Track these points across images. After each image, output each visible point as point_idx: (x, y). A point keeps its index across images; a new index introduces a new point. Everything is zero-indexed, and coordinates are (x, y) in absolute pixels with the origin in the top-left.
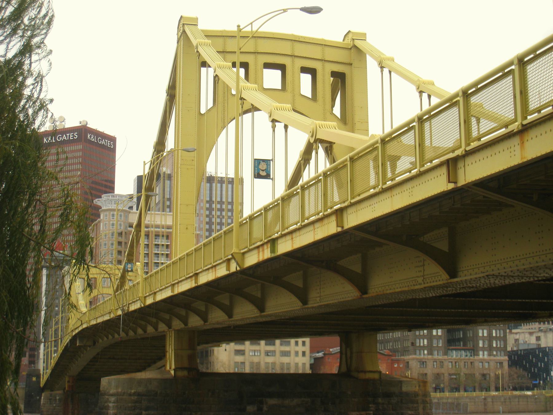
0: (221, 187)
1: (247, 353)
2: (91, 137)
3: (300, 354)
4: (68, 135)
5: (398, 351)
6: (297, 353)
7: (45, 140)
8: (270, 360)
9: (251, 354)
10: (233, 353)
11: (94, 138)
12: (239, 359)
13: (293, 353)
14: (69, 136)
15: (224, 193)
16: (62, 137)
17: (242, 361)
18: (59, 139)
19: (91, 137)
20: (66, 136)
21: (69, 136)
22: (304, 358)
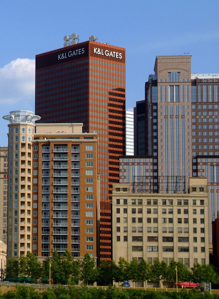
0: (213, 98)
1: (144, 249)
2: (97, 50)
3: (199, 250)
4: (77, 50)
5: (80, 279)
6: (195, 249)
7: (59, 57)
8: (154, 255)
9: (148, 250)
10: (130, 249)
11: (101, 51)
12: (137, 254)
13: (191, 249)
14: (78, 51)
15: (123, 68)
16: (72, 53)
17: (141, 256)
18: (70, 55)
19: (97, 50)
20: (76, 52)
21: (78, 51)
22: (203, 254)
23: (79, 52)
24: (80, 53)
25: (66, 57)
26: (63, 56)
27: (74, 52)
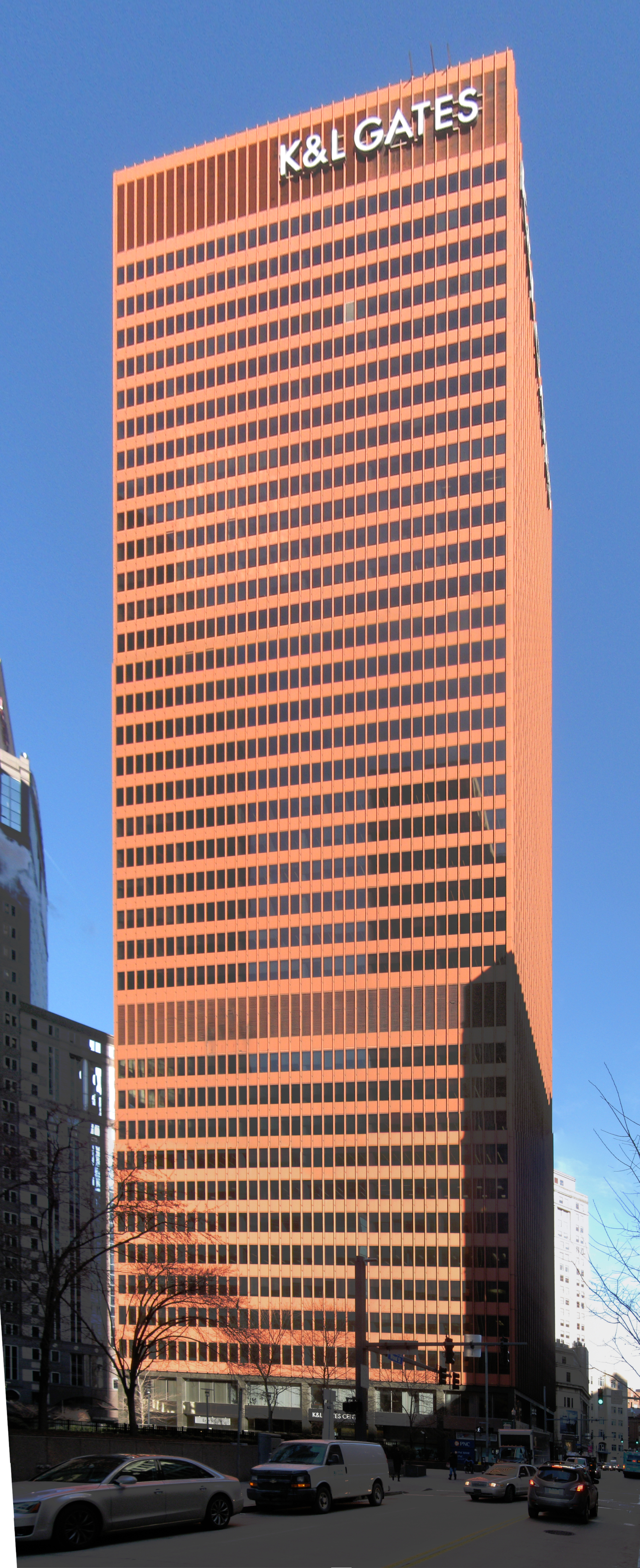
23: (439, 113)
24: (444, 118)
25: (336, 156)
26: (312, 149)
27: (399, 116)
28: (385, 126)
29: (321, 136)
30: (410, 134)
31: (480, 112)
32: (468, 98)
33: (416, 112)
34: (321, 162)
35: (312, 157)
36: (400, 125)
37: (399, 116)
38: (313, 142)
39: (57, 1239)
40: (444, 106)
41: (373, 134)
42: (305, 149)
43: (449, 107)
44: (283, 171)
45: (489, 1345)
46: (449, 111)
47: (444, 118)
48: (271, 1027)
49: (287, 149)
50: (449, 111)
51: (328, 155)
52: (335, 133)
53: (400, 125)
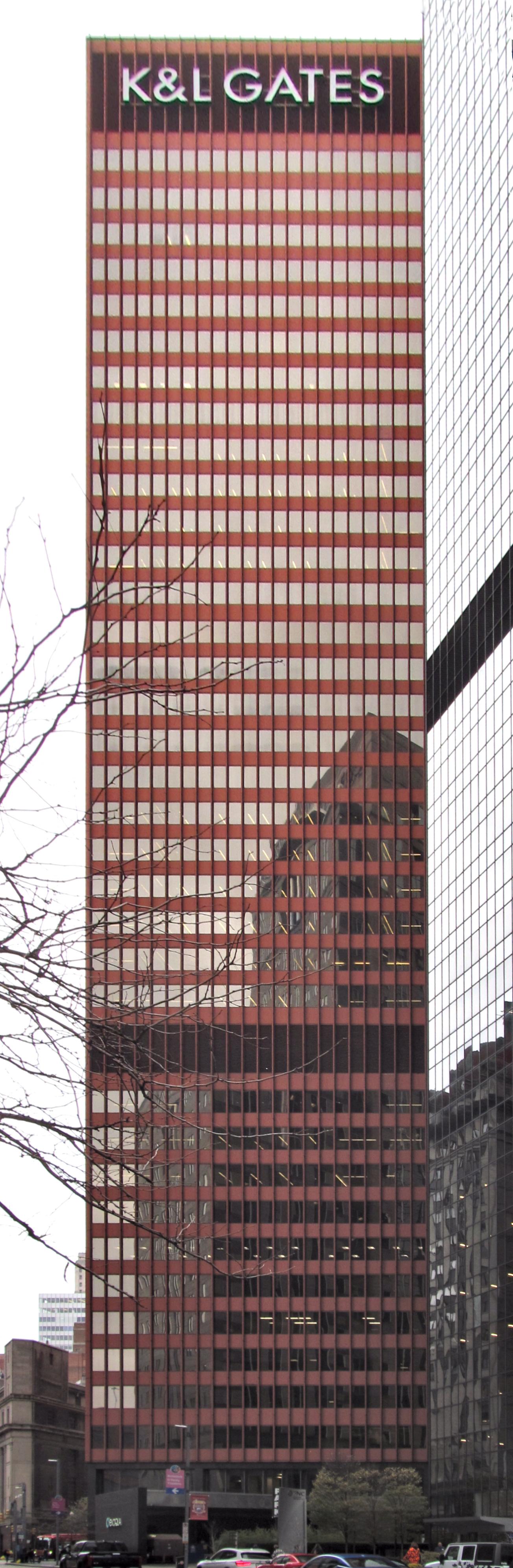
23: (334, 86)
24: (340, 93)
27: (283, 75)
28: (265, 82)
29: (177, 71)
30: (298, 98)
31: (386, 96)
32: (371, 78)
33: (305, 77)
34: (177, 99)
35: (165, 92)
36: (283, 85)
37: (283, 75)
38: (168, 75)
39: (11, 1109)
40: (340, 79)
41: (249, 87)
42: (157, 81)
43: (348, 82)
44: (126, 97)
45: (399, 1366)
46: (347, 86)
47: (340, 93)
48: (409, 100)
49: (132, 74)
50: (347, 86)
51: (189, 93)
52: (196, 74)
53: (283, 85)
